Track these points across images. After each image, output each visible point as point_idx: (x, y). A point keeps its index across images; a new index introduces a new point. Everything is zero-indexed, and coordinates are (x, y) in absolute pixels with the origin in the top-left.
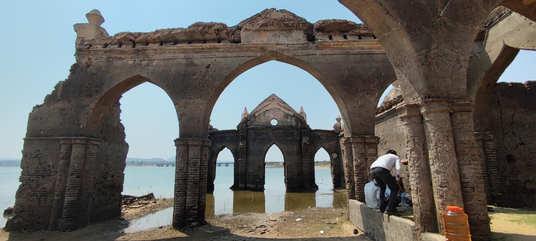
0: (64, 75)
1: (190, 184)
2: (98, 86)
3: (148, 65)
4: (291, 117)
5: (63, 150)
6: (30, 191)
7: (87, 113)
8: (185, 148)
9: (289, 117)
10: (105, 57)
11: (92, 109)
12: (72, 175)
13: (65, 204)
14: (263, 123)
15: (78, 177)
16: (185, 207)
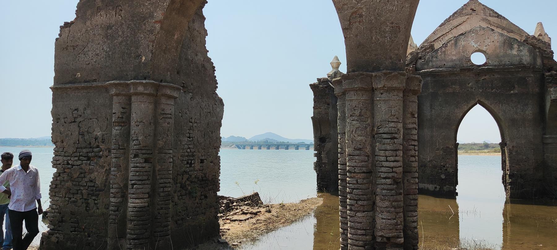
1: (383, 186)
4: (520, 44)
5: (116, 108)
6: (69, 184)
7: (151, 32)
8: (365, 97)
9: (516, 46)
11: (160, 22)
12: (136, 156)
13: (130, 212)
14: (452, 61)
15: (146, 161)
16: (374, 238)
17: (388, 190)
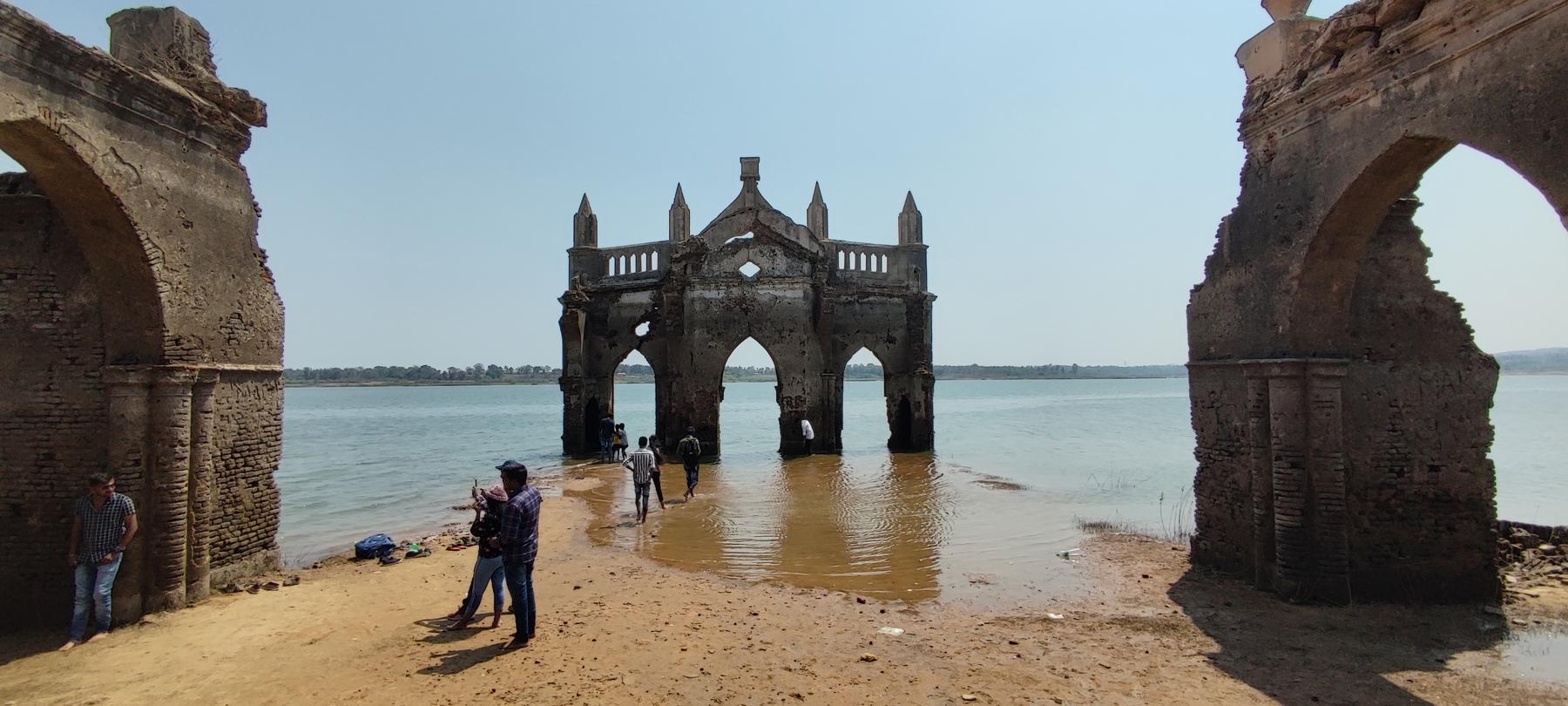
0: (1227, 197)
2: (1299, 209)
3: (1432, 89)
5: (1252, 395)
6: (1212, 483)
7: (1287, 292)
10: (1303, 115)
12: (1278, 458)
15: (1293, 465)
17: (760, 557)
